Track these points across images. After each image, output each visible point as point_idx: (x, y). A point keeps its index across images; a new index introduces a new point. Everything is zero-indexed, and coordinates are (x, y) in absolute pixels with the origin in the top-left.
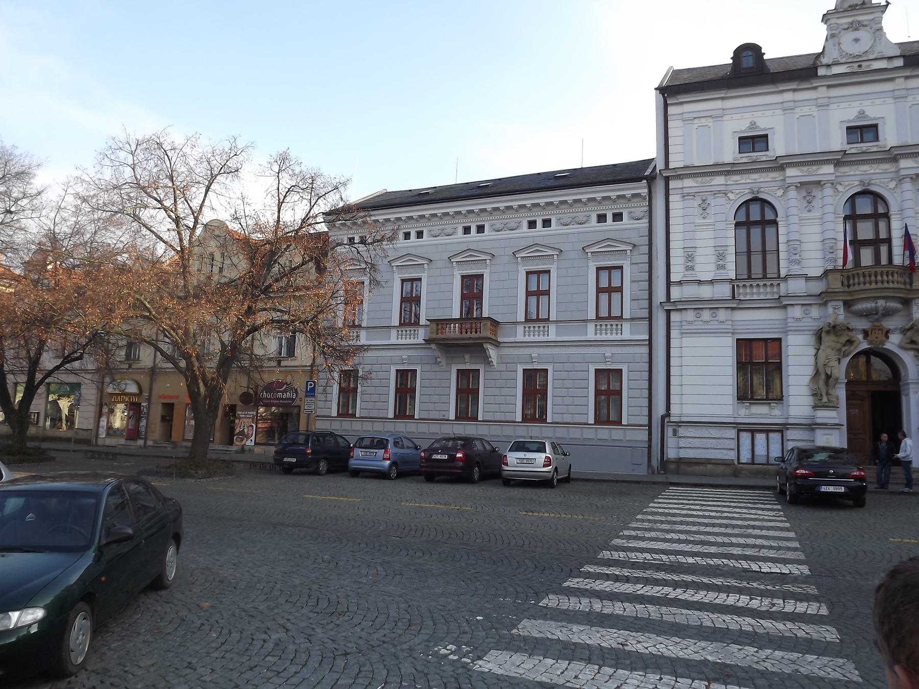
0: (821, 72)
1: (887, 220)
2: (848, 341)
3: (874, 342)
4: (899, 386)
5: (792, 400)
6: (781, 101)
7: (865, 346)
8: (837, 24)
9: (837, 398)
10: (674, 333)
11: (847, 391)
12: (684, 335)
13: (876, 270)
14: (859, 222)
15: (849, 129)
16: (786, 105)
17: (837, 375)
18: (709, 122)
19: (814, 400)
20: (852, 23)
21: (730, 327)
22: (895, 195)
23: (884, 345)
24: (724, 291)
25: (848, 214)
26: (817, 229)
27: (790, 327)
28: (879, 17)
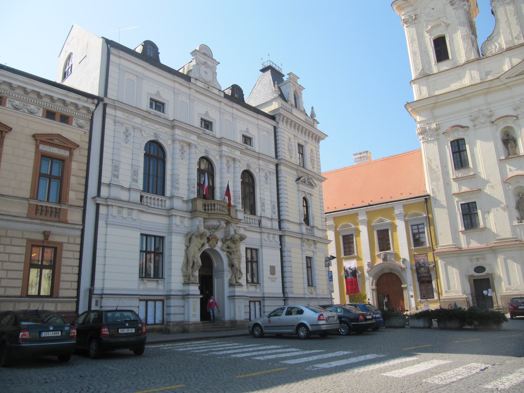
4: (212, 272)
10: (101, 223)
24: (136, 197)
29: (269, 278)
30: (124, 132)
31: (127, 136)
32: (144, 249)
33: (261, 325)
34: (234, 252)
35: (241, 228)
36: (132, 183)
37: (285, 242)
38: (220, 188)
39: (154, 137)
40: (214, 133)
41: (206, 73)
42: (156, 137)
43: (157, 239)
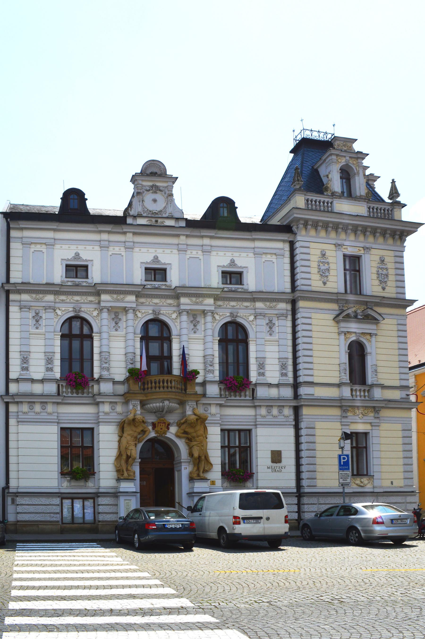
0: (129, 221)
1: (169, 342)
2: (142, 431)
3: (159, 432)
4: (173, 464)
5: (102, 475)
6: (99, 239)
7: (153, 434)
8: (142, 185)
9: (134, 473)
10: (12, 422)
11: (140, 468)
12: (20, 423)
13: (163, 378)
14: (151, 342)
15: (223, 272)
16: (102, 243)
17: (135, 456)
18: (43, 248)
19: (118, 475)
20: (152, 186)
21: (219, 419)
22: (176, 323)
23: (166, 434)
24: (52, 388)
25: (143, 335)
26: (201, 347)
27: (101, 419)
28: (170, 186)
29: (268, 468)
30: (33, 317)
31: (37, 321)
32: (227, 444)
33: (310, 525)
34: (194, 437)
35: (212, 405)
36: (259, 378)
37: (302, 415)
38: (204, 357)
39: (230, 317)
40: (245, 287)
41: (155, 201)
42: (233, 317)
43: (242, 434)
